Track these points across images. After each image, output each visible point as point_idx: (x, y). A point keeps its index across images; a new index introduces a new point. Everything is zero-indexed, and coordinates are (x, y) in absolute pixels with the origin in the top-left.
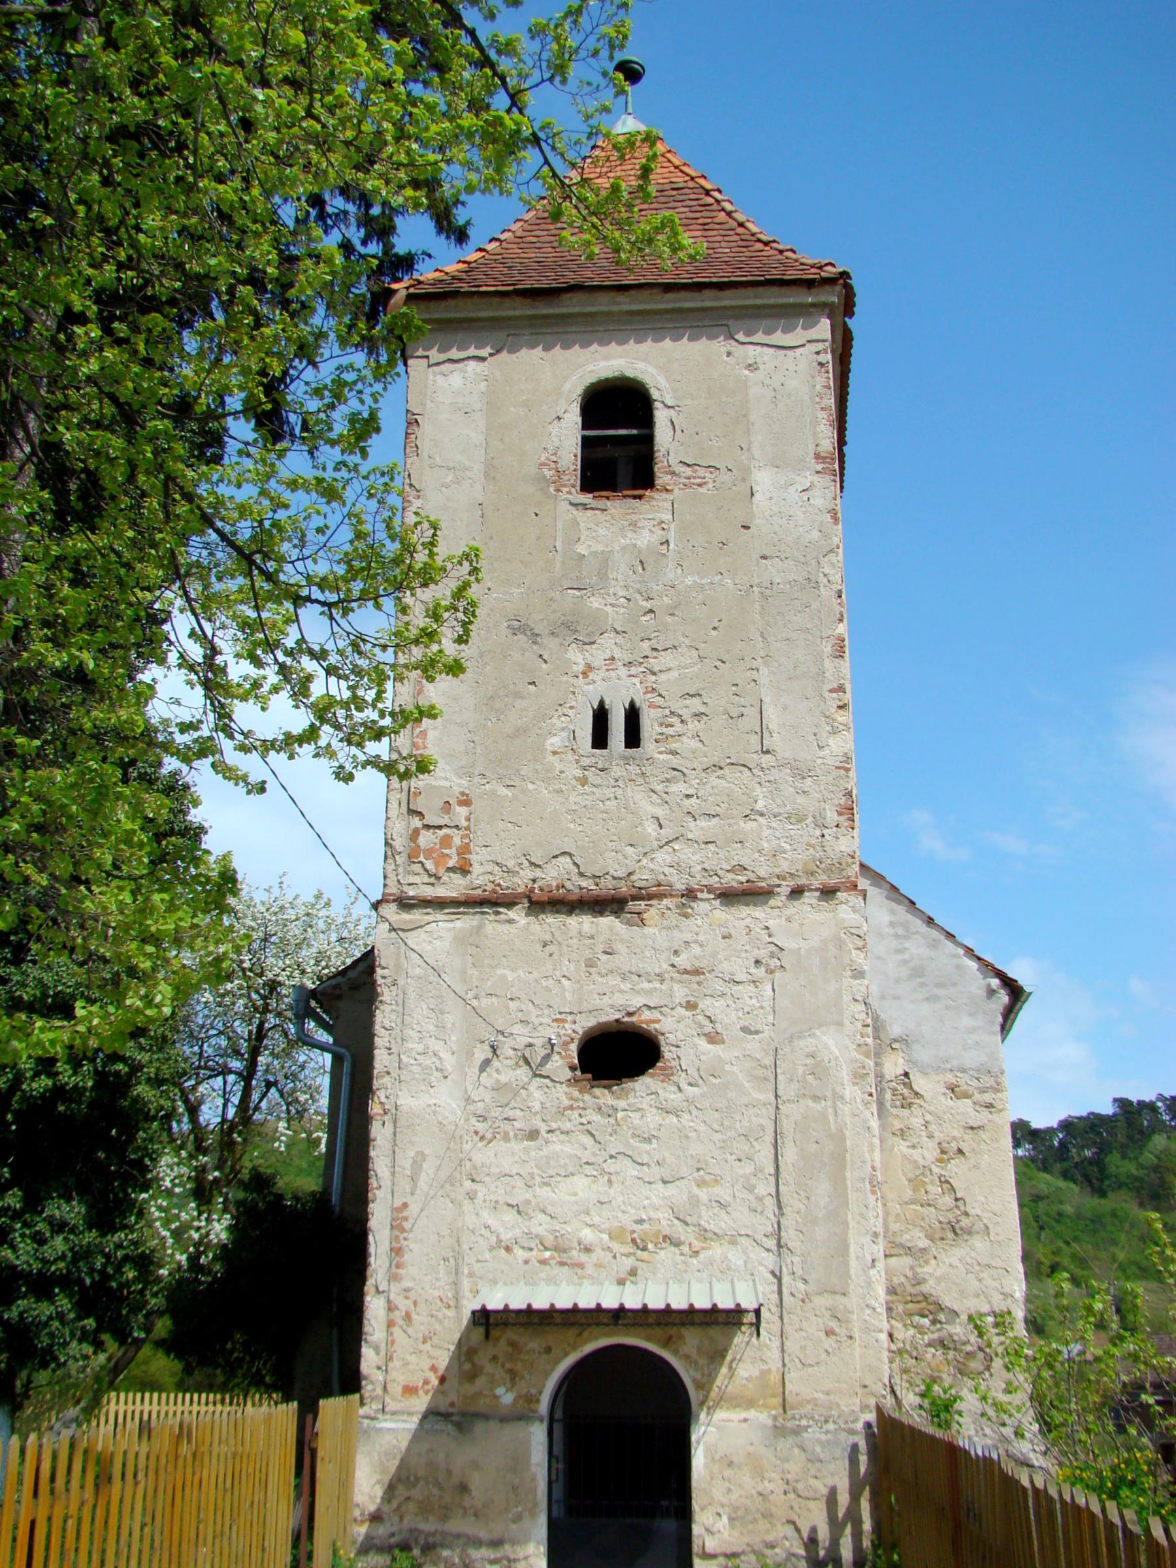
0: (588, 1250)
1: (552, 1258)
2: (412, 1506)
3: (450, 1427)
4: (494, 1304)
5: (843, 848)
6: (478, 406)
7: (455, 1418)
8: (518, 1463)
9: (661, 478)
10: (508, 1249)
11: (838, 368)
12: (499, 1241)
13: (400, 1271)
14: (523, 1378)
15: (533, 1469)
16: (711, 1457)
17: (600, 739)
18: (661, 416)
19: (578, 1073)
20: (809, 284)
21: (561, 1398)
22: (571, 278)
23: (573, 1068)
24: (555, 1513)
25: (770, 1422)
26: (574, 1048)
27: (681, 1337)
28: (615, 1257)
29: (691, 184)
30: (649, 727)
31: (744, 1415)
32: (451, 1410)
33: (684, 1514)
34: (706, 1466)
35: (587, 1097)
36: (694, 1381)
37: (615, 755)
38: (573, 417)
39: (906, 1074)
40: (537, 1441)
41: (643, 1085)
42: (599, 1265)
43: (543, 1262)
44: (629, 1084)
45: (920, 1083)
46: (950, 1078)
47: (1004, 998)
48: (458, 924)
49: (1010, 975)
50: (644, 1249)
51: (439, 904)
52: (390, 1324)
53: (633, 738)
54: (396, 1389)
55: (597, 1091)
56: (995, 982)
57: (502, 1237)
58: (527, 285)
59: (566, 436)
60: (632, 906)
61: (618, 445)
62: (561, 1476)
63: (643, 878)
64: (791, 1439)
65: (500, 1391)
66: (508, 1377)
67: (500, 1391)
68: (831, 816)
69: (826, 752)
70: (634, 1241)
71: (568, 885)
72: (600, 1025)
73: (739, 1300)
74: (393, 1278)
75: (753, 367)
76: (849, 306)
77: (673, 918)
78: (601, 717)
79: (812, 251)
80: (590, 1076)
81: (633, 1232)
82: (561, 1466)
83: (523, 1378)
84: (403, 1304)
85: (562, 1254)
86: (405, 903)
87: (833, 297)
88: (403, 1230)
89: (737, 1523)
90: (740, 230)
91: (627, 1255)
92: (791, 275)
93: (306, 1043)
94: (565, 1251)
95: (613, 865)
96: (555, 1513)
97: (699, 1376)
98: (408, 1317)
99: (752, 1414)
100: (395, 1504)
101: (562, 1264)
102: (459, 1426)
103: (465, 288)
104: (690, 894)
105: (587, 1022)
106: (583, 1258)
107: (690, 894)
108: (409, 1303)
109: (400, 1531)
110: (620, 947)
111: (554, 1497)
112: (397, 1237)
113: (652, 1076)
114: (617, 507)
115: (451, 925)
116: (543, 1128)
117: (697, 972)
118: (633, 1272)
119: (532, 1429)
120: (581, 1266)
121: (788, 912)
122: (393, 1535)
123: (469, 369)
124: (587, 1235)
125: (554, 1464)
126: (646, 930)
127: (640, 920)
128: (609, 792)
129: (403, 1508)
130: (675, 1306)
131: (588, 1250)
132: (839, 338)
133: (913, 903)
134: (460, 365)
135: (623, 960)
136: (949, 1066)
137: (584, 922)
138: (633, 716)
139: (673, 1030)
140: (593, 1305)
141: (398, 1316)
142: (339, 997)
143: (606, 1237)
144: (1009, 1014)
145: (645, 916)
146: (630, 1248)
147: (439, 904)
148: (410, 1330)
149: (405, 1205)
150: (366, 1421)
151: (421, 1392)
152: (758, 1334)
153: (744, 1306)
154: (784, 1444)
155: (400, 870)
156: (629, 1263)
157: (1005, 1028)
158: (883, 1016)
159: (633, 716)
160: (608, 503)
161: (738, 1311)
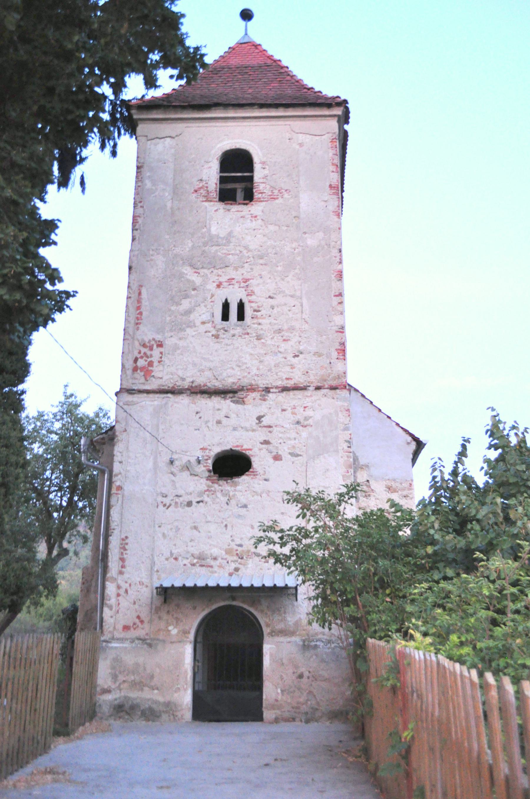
0: (215, 559)
1: (197, 562)
2: (125, 685)
3: (145, 646)
4: (167, 584)
5: (340, 369)
7: (148, 641)
8: (178, 663)
9: (256, 195)
10: (176, 559)
12: (172, 554)
13: (123, 569)
14: (182, 621)
16: (273, 659)
17: (225, 317)
18: (257, 167)
19: (212, 474)
21: (201, 632)
22: (215, 100)
23: (209, 471)
24: (196, 688)
25: (301, 643)
26: (210, 463)
27: (259, 601)
28: (228, 562)
29: (274, 64)
30: (248, 312)
31: (289, 639)
32: (147, 637)
33: (259, 688)
34: (271, 664)
35: (216, 486)
36: (266, 622)
37: (232, 324)
38: (215, 166)
39: (368, 481)
41: (244, 479)
42: (220, 566)
43: (193, 565)
44: (236, 480)
48: (156, 403)
50: (242, 558)
51: (148, 392)
52: (118, 595)
53: (241, 316)
54: (120, 627)
56: (410, 439)
57: (173, 551)
59: (211, 174)
61: (237, 176)
63: (245, 382)
64: (312, 652)
65: (170, 628)
67: (170, 628)
68: (335, 354)
69: (333, 323)
70: (237, 554)
71: (208, 384)
74: (121, 573)
75: (301, 145)
77: (258, 401)
78: (226, 306)
79: (329, 92)
82: (200, 664)
83: (182, 621)
84: (125, 586)
85: (202, 560)
87: (339, 111)
88: (125, 550)
89: (285, 693)
90: (296, 84)
91: (234, 561)
92: (319, 101)
93: (341, 713)
94: (204, 559)
95: (230, 378)
96: (196, 688)
98: (126, 591)
99: (293, 639)
101: (202, 566)
102: (150, 645)
103: (165, 103)
104: (267, 390)
105: (217, 450)
106: (212, 563)
107: (267, 390)
108: (127, 585)
109: (120, 698)
110: (233, 416)
111: (197, 680)
113: (247, 475)
114: (236, 210)
115: (152, 403)
116: (194, 501)
117: (270, 427)
118: (237, 570)
119: (186, 647)
120: (212, 567)
123: (166, 143)
124: (215, 551)
125: (197, 663)
126: (245, 406)
128: (229, 342)
129: (122, 686)
130: (255, 585)
131: (215, 559)
132: (342, 135)
134: (162, 140)
135: (233, 421)
136: (387, 478)
137: (216, 401)
138: (241, 306)
140: (215, 585)
141: (122, 592)
142: (104, 444)
143: (224, 553)
145: (245, 399)
146: (235, 558)
147: (148, 392)
148: (127, 598)
149: (127, 537)
150: (104, 644)
151: (132, 629)
152: (297, 600)
154: (308, 654)
155: (129, 377)
156: (233, 566)
159: (241, 306)
160: (231, 206)
161: (286, 587)
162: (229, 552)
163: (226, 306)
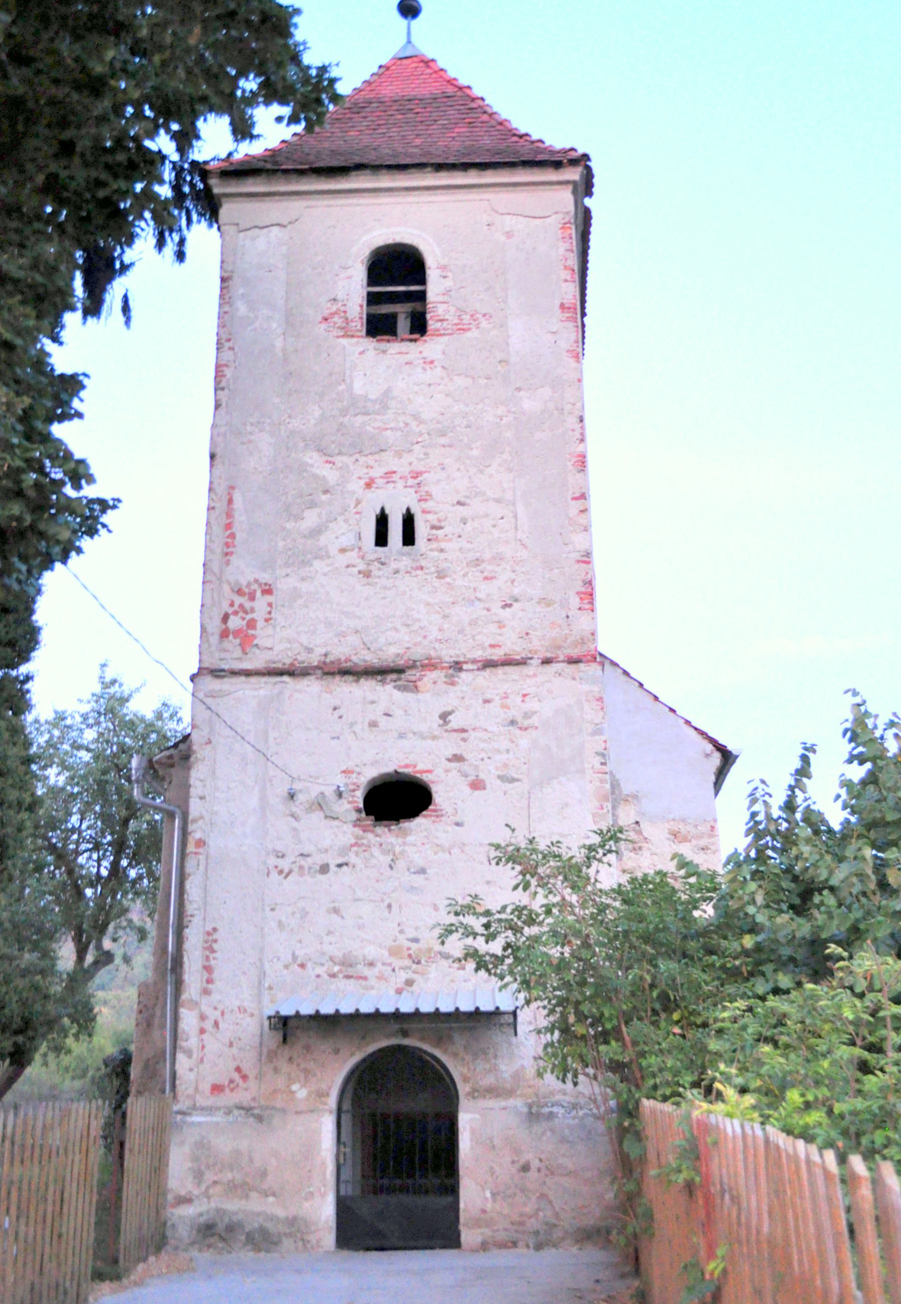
1: (340, 971)
6: (281, 266)
7: (256, 1111)
8: (310, 1149)
9: (432, 325)
10: (302, 966)
11: (580, 243)
14: (315, 1075)
15: (324, 1154)
16: (476, 1139)
17: (381, 539)
19: (363, 815)
20: (557, 165)
22: (357, 159)
23: (358, 811)
24: (342, 1193)
25: (525, 1110)
28: (394, 970)
29: (459, 93)
31: (503, 1104)
32: (253, 1104)
33: (452, 1190)
35: (370, 836)
36: (462, 1074)
38: (360, 274)
40: (324, 1131)
41: (420, 824)
42: (381, 977)
43: (333, 976)
44: (406, 824)
45: (647, 829)
46: (675, 827)
47: (717, 756)
48: (262, 692)
49: (721, 742)
50: (419, 963)
51: (248, 673)
52: (202, 1031)
53: (409, 538)
54: (206, 1087)
55: (379, 830)
56: (710, 747)
58: (321, 164)
59: (353, 288)
60: (410, 675)
61: (397, 286)
62: (349, 1162)
63: (418, 653)
64: (545, 1124)
65: (295, 1087)
66: (302, 1076)
68: (575, 602)
70: (410, 956)
72: (383, 776)
73: (498, 1004)
74: (206, 992)
75: (509, 235)
76: (586, 186)
77: (441, 686)
78: (382, 521)
79: (557, 140)
80: (372, 818)
81: (409, 949)
82: (348, 1150)
83: (315, 1075)
84: (213, 1015)
85: (347, 968)
86: (217, 673)
87: (574, 174)
90: (499, 127)
92: (540, 157)
94: (351, 966)
97: (465, 1071)
98: (216, 1024)
99: (511, 1102)
100: (203, 1187)
101: (349, 977)
103: (269, 166)
104: (457, 666)
106: (366, 971)
107: (457, 666)
109: (208, 1212)
110: (398, 712)
112: (207, 958)
113: (424, 816)
117: (463, 731)
119: (323, 1119)
120: (365, 978)
121: (539, 679)
122: (201, 1215)
123: (272, 235)
124: (371, 952)
125: (342, 1149)
126: (420, 696)
127: (413, 687)
133: (641, 685)
135: (399, 722)
136: (671, 816)
137: (368, 686)
138: (409, 521)
139: (445, 791)
141: (208, 1025)
144: (721, 774)
146: (407, 962)
147: (248, 673)
149: (215, 930)
150: (179, 1117)
153: (503, 1008)
154: (537, 1129)
156: (403, 976)
157: (718, 785)
158: (618, 776)
159: (409, 521)
160: (388, 345)
162: (394, 952)
163: (382, 521)
